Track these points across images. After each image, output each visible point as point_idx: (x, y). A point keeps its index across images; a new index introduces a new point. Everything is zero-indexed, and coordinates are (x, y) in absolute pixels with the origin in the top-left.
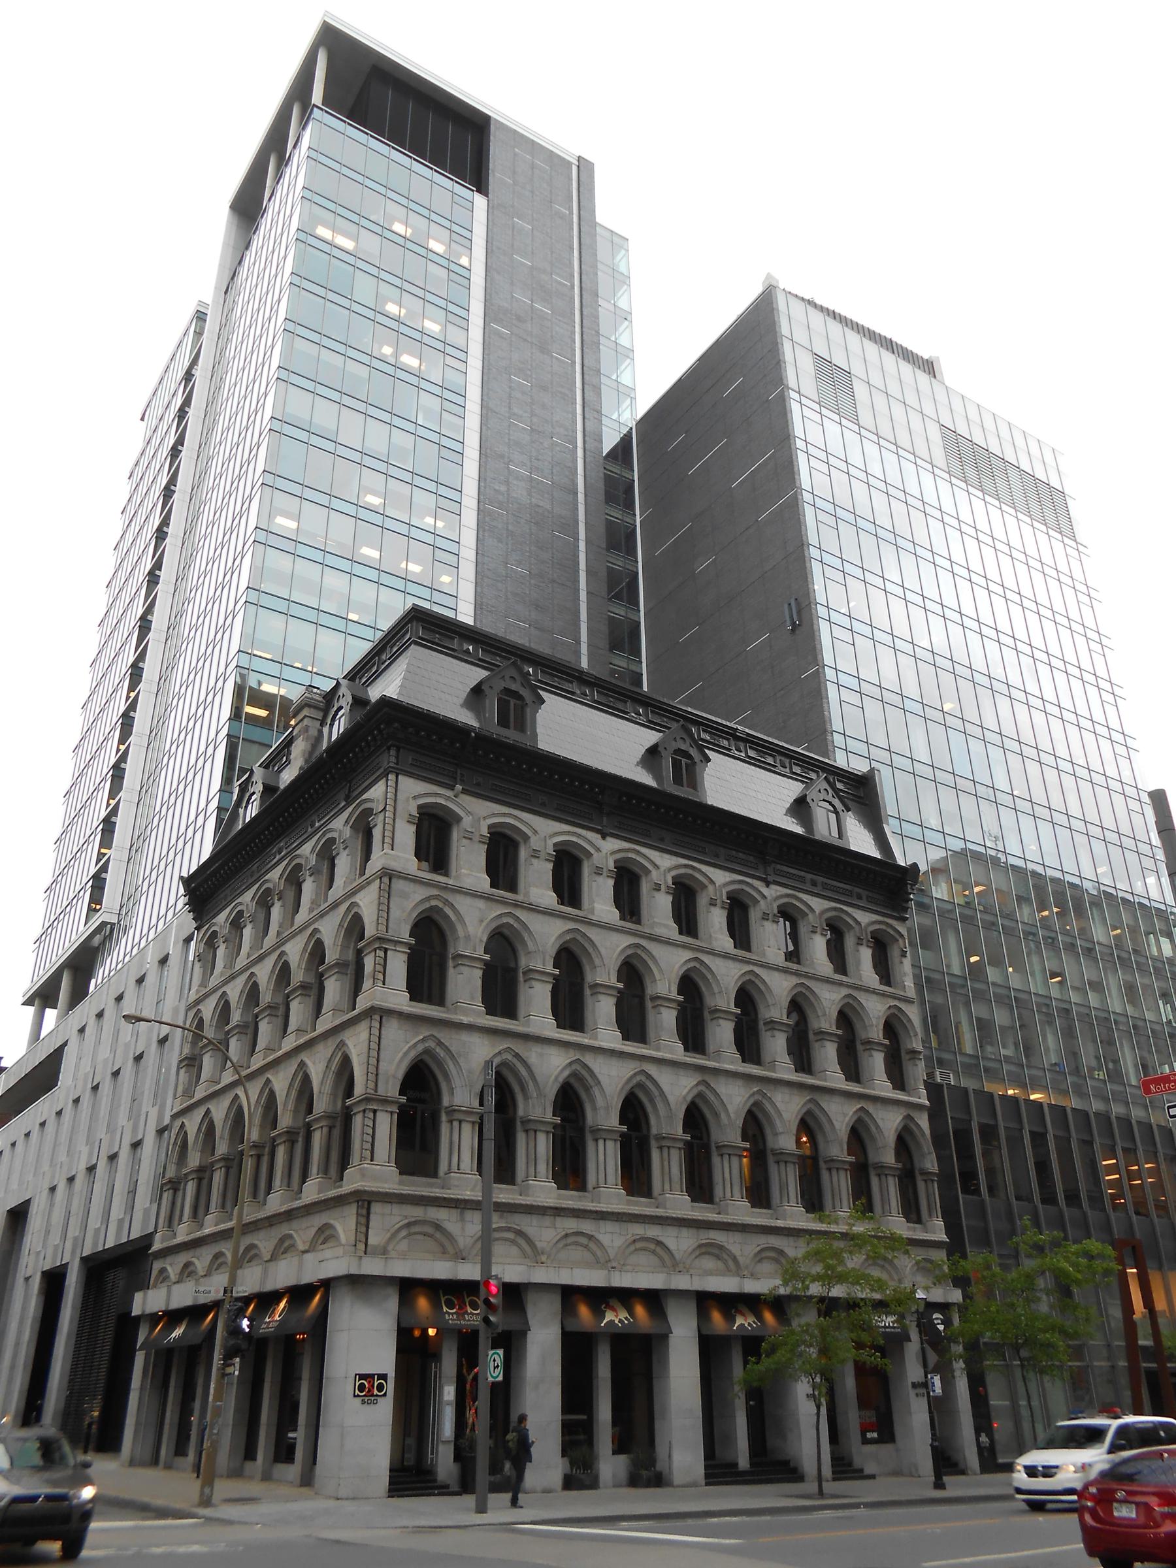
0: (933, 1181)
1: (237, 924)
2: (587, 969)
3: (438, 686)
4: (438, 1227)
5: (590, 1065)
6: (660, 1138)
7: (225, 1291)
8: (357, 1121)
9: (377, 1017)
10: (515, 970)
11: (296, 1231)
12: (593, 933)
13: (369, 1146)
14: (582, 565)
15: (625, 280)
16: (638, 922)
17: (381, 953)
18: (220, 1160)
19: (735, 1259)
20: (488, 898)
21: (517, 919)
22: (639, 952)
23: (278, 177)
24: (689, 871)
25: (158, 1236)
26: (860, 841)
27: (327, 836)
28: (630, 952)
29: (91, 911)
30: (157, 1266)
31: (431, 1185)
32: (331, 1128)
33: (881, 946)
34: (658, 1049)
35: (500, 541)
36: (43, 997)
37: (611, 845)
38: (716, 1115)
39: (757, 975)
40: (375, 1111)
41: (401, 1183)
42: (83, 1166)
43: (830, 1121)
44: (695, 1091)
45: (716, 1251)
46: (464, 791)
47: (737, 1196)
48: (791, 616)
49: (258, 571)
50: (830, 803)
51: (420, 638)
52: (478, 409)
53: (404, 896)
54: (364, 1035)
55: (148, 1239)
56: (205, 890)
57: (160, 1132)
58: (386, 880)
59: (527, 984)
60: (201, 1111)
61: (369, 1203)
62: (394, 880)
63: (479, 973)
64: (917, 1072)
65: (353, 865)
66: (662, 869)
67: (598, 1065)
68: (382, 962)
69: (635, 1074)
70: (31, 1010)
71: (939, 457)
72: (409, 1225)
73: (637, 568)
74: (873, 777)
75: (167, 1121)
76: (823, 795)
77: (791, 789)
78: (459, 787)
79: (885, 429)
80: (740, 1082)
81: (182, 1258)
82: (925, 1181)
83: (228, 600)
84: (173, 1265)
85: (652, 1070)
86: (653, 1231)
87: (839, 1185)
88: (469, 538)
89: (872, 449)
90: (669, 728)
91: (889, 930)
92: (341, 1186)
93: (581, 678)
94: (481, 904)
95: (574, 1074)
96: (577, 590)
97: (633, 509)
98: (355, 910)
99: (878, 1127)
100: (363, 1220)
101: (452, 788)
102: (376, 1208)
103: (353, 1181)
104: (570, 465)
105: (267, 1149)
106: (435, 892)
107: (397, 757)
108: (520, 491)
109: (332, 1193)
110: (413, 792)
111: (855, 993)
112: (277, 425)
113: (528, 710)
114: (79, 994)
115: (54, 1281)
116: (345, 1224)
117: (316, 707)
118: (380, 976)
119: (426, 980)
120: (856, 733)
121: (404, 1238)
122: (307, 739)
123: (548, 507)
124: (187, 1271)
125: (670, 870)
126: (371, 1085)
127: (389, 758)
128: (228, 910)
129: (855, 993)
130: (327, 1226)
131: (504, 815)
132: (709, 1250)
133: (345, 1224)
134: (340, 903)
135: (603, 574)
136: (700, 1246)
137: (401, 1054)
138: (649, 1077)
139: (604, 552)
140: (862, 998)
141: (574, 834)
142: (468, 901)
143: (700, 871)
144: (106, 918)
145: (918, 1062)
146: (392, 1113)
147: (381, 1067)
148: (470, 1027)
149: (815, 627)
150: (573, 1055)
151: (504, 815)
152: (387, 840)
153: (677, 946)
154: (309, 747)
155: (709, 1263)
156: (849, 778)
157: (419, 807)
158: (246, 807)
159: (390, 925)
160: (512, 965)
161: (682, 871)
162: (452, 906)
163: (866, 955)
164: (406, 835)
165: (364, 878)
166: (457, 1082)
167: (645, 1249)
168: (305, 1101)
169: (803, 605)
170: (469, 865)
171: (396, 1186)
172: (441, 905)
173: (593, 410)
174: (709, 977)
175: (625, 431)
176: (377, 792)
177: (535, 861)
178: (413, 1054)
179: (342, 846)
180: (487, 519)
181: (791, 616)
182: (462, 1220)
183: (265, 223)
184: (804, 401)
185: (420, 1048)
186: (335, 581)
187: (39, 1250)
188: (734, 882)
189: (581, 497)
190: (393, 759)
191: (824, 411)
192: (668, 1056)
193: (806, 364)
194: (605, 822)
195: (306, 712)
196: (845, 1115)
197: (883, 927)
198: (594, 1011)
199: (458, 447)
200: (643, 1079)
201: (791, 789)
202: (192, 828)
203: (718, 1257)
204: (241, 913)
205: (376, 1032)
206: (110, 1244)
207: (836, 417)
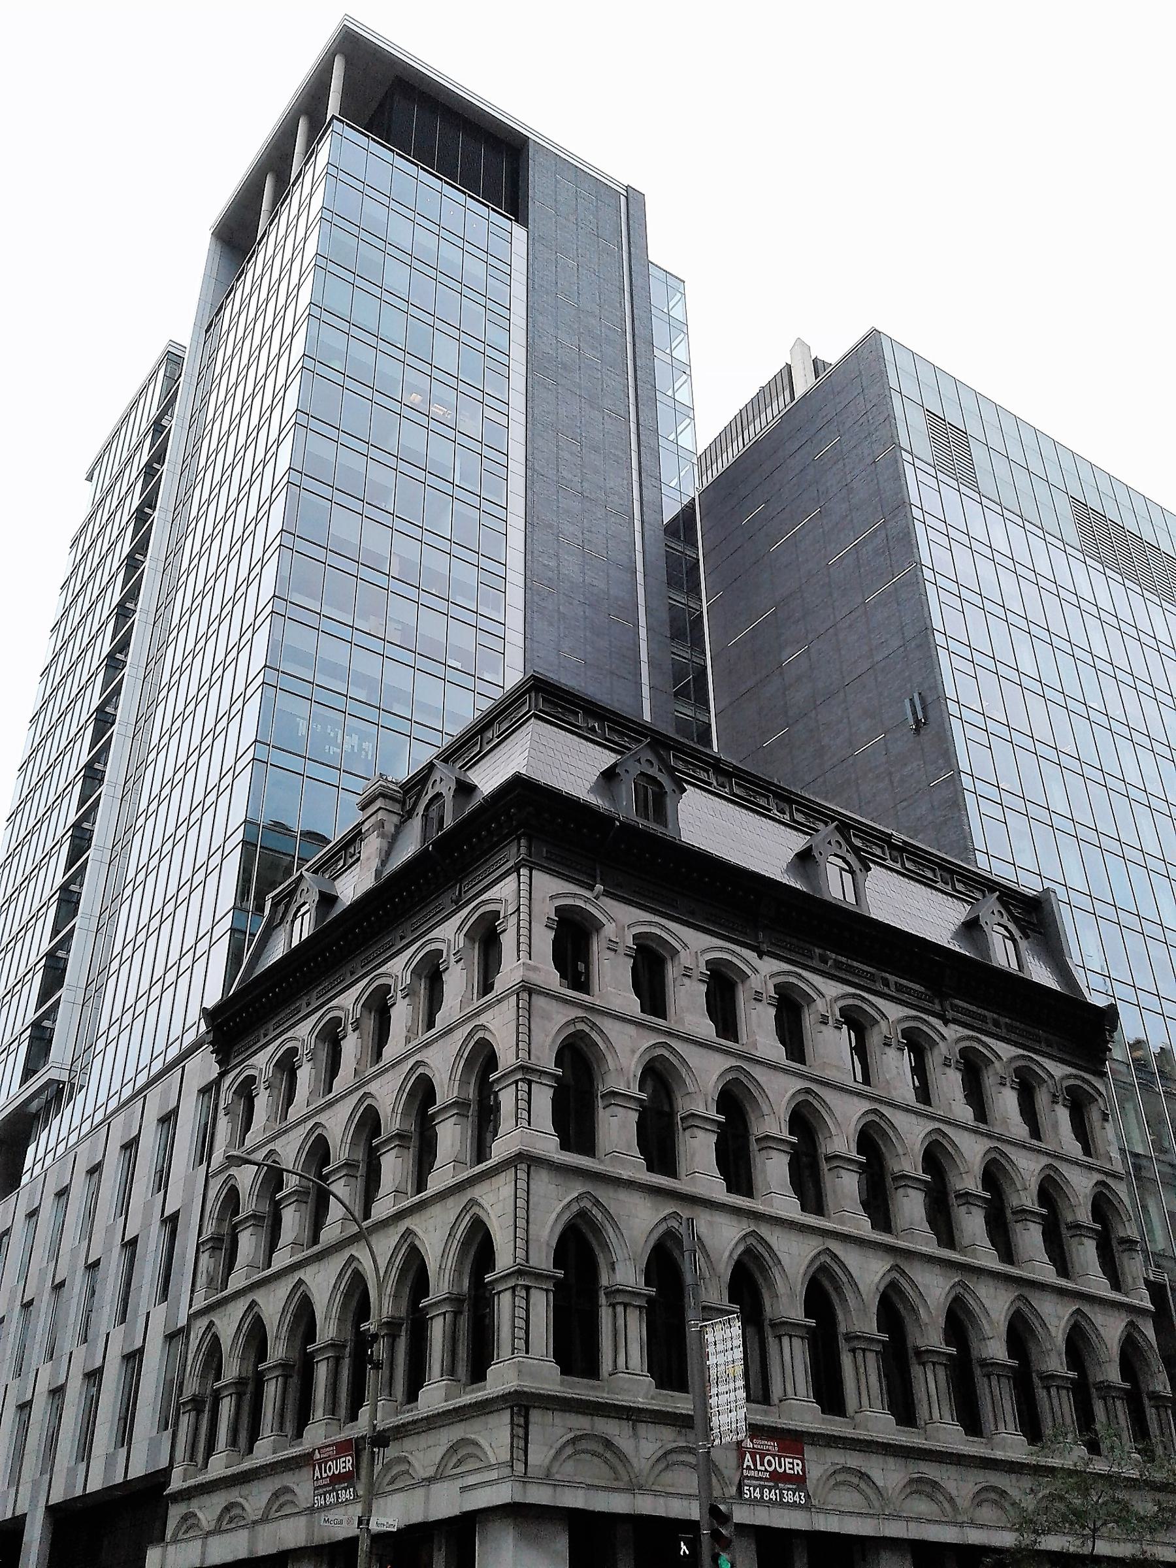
0: (1166, 1407)
1: (287, 1066)
2: (752, 1117)
3: (571, 765)
4: (608, 1444)
5: (768, 1239)
6: (849, 1338)
7: (360, 1522)
8: (504, 1303)
9: (524, 1166)
10: (672, 1114)
11: (200, 1508)
12: (758, 1072)
13: (522, 1334)
14: (644, 656)
15: (682, 327)
16: (802, 1061)
17: (523, 1086)
18: (275, 1367)
19: (951, 1500)
20: (639, 1024)
21: (673, 1050)
22: (810, 1099)
23: (274, 214)
24: (859, 1003)
25: (177, 1473)
26: (1041, 974)
27: (433, 946)
28: (800, 1098)
29: (29, 1072)
30: (175, 1512)
31: (593, 1388)
32: (457, 1314)
33: (1079, 1104)
34: (842, 1223)
35: (551, 624)
37: (769, 965)
38: (914, 1310)
39: (945, 1135)
40: (528, 1289)
41: (562, 1383)
42: (43, 1387)
43: (1044, 1325)
44: (888, 1279)
45: (928, 1489)
46: (606, 893)
47: (947, 1418)
48: (915, 713)
49: (273, 647)
50: (1006, 928)
51: (540, 711)
52: (521, 470)
53: (547, 1017)
54: (507, 1191)
55: (164, 1475)
56: (233, 1025)
57: (170, 1337)
58: (525, 996)
59: (688, 1132)
60: (241, 1305)
61: (527, 1409)
62: (534, 997)
63: (635, 1116)
64: (1135, 1268)
65: (469, 980)
66: (828, 998)
67: (778, 1240)
68: (526, 1096)
69: (819, 1254)
71: (1071, 535)
72: (574, 1441)
73: (705, 660)
74: (1048, 900)
75: (182, 1321)
76: (997, 918)
77: (958, 912)
78: (599, 887)
79: (1009, 500)
80: (937, 1269)
81: (219, 1500)
82: (1157, 1408)
83: (234, 681)
84: (207, 1511)
85: (836, 1247)
86: (854, 1460)
87: (1058, 1408)
88: (515, 620)
89: (995, 522)
90: (817, 831)
91: (1085, 1086)
92: (301, 1444)
93: (716, 766)
94: (631, 1030)
95: (748, 1251)
96: (639, 685)
97: (699, 594)
99: (1099, 1335)
100: (521, 1432)
101: (591, 888)
102: (535, 1416)
103: (501, 1378)
104: (627, 539)
105: (348, 1349)
106: (581, 1013)
107: (529, 848)
108: (571, 566)
109: (467, 1399)
110: (551, 890)
111: (1057, 1164)
112: (295, 477)
113: (668, 801)
116: (494, 1438)
117: (392, 798)
118: (525, 1115)
119: (575, 1120)
120: (1006, 848)
121: (569, 1457)
122: (382, 835)
123: (603, 586)
124: (230, 1518)
125: (837, 999)
126: (521, 1253)
127: (514, 852)
128: (271, 1048)
129: (1057, 1164)
130: (287, 1490)
131: (650, 923)
132: (922, 1487)
133: (494, 1438)
134: (457, 1027)
135: (668, 666)
136: (912, 1481)
137: (554, 1215)
138: (835, 1257)
139: (668, 641)
140: (1063, 1168)
141: (728, 950)
142: (618, 1025)
143: (873, 1005)
144: (54, 1074)
145: (1134, 1255)
146: (547, 1291)
147: (531, 1232)
148: (630, 1184)
149: (947, 726)
150: (746, 1226)
151: (650, 923)
152: (523, 947)
153: (851, 1092)
154: (385, 846)
155: (922, 1506)
156: (1022, 902)
157: (558, 910)
158: (293, 922)
159: (533, 1051)
160: (666, 1108)
161: (850, 1001)
162: (601, 1032)
163: (1063, 1115)
164: (544, 940)
166: (619, 1253)
167: (843, 1483)
169: (929, 700)
170: (613, 982)
171: (558, 1388)
172: (587, 1030)
173: (650, 474)
174: (891, 1133)
175: (686, 501)
176: (505, 891)
177: (686, 981)
178: (566, 1217)
179: (453, 959)
180: (536, 598)
181: (915, 713)
182: (635, 1435)
184: (918, 463)
185: (575, 1208)
186: (366, 665)
188: (907, 1018)
189: (640, 577)
190: (523, 850)
191: (941, 476)
192: (855, 1232)
193: (917, 420)
194: (761, 935)
195: (379, 803)
196: (1060, 1318)
197: (1079, 1082)
198: (764, 1171)
199: (500, 513)
200: (828, 1260)
201: (958, 912)
203: (931, 1497)
204: (293, 1051)
205: (522, 1184)
206: (94, 1485)
207: (954, 484)
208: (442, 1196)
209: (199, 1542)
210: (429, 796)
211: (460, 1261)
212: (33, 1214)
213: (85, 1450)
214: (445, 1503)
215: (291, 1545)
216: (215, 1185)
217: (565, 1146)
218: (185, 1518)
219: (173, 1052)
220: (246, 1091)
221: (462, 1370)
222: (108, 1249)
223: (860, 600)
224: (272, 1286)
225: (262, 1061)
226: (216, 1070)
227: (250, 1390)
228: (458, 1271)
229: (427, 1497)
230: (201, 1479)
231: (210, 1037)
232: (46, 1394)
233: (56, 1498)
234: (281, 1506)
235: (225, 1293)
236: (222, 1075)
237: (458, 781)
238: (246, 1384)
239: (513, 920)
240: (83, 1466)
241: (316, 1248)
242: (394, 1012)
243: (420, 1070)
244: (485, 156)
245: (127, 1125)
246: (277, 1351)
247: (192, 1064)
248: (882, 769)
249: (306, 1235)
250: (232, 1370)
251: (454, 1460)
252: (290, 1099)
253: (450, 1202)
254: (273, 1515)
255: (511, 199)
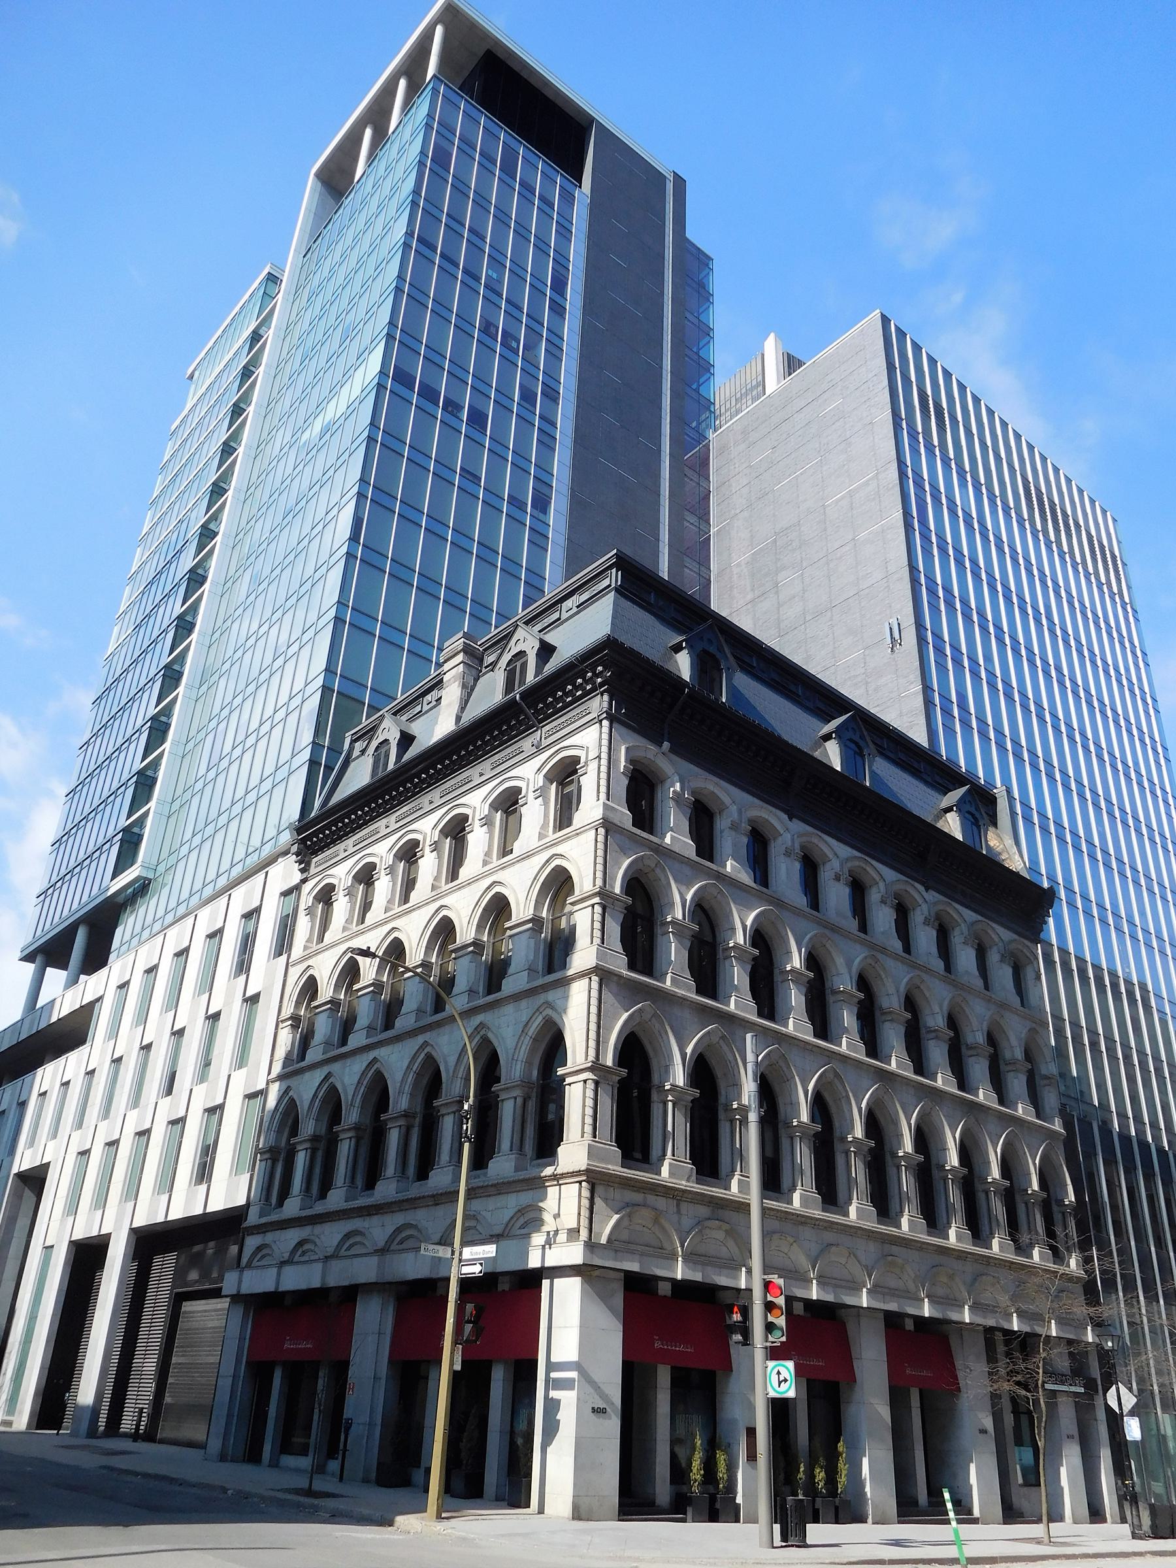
18: (349, 1130)
23: (428, 36)
36: (50, 952)
70: (30, 968)
81: (292, 1236)
98: (311, 972)
101: (660, 745)
114: (96, 960)
115: (87, 1257)
165: (362, 927)
168: (290, 1122)
170: (676, 835)
183: (351, 201)
187: (55, 1230)
202: (199, 836)
208: (516, 997)
209: (320, 1265)
210: (513, 652)
211: (532, 1051)
212: (124, 986)
213: (204, 1172)
214: (340, 1275)
215: (362, 1280)
216: (295, 972)
217: (632, 966)
218: (259, 1249)
219: (222, 882)
220: (326, 896)
221: (359, 1182)
222: (228, 1002)
223: (851, 537)
224: (348, 1061)
225: (342, 874)
226: (297, 877)
227: (325, 1147)
228: (529, 1063)
229: (279, 1274)
230: (274, 1217)
231: (295, 848)
232: (241, 1098)
233: (78, 1235)
234: (263, 1257)
235: (303, 1064)
236: (304, 881)
237: (542, 642)
238: (415, 1118)
239: (593, 766)
240: (71, 1219)
241: (390, 1034)
242: (471, 838)
243: (497, 889)
244: (549, 125)
245: (213, 918)
246: (308, 1128)
247: (276, 871)
248: (859, 679)
249: (379, 1024)
250: (308, 1128)
251: (259, 1256)
252: (366, 906)
253: (524, 1003)
254: (343, 1252)
255: (570, 164)
